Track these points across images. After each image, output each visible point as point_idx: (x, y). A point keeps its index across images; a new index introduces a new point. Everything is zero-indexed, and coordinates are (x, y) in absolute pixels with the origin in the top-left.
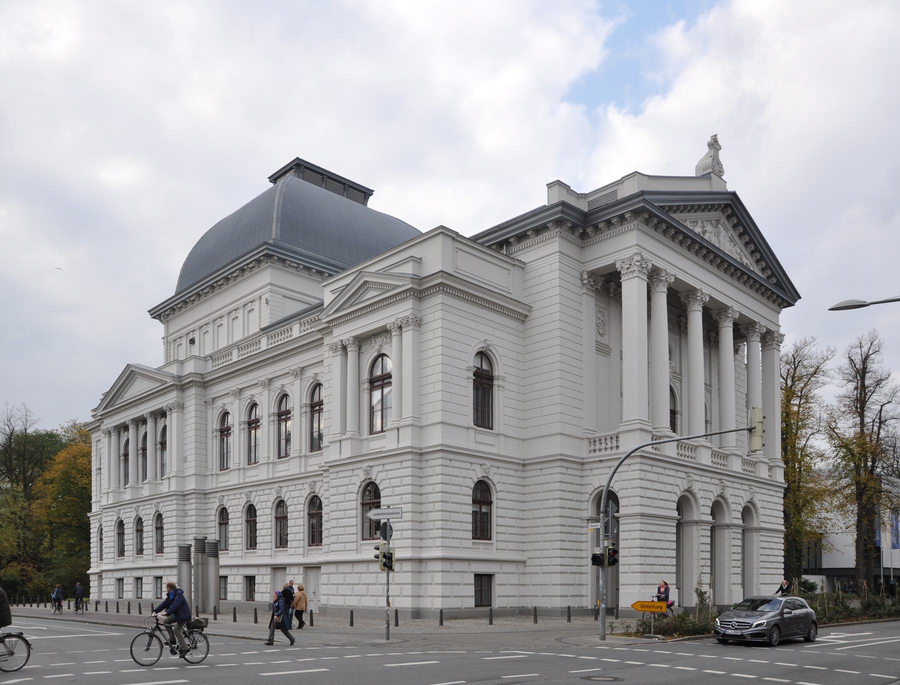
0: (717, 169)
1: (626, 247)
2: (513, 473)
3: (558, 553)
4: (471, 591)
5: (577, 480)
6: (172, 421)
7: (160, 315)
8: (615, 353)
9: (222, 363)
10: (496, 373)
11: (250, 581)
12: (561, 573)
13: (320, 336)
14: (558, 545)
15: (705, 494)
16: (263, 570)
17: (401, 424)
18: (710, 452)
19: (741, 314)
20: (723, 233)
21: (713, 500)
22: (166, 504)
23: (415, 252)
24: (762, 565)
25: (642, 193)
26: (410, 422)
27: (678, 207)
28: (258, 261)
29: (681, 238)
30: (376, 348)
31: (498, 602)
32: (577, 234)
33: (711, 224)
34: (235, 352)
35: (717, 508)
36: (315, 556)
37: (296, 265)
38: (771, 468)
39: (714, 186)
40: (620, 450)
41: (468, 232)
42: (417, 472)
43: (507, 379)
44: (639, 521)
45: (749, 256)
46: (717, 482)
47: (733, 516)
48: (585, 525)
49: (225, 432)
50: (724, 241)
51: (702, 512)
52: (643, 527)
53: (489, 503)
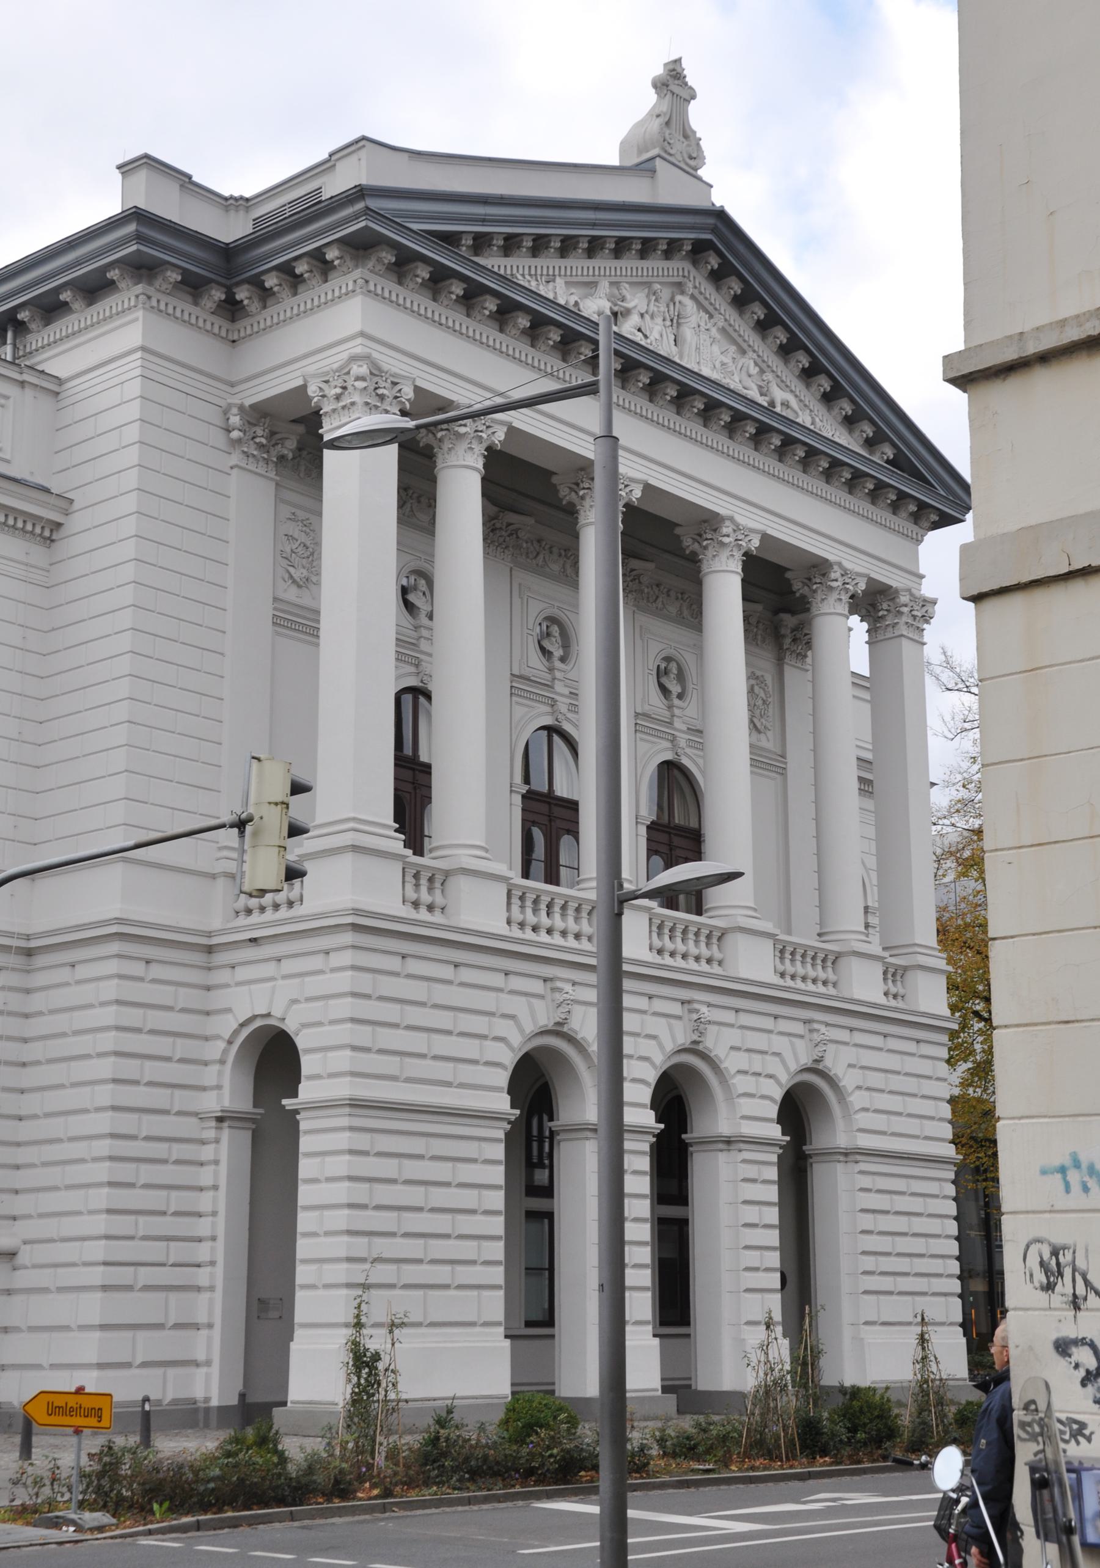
0: (679, 147)
1: (343, 337)
3: (100, 1224)
5: (186, 997)
12: (105, 1288)
14: (101, 1198)
24: (869, 1263)
32: (253, 306)
38: (894, 974)
39: (669, 189)
44: (345, 1122)
46: (676, 1009)
48: (211, 1134)
50: (709, 345)
52: (362, 1141)
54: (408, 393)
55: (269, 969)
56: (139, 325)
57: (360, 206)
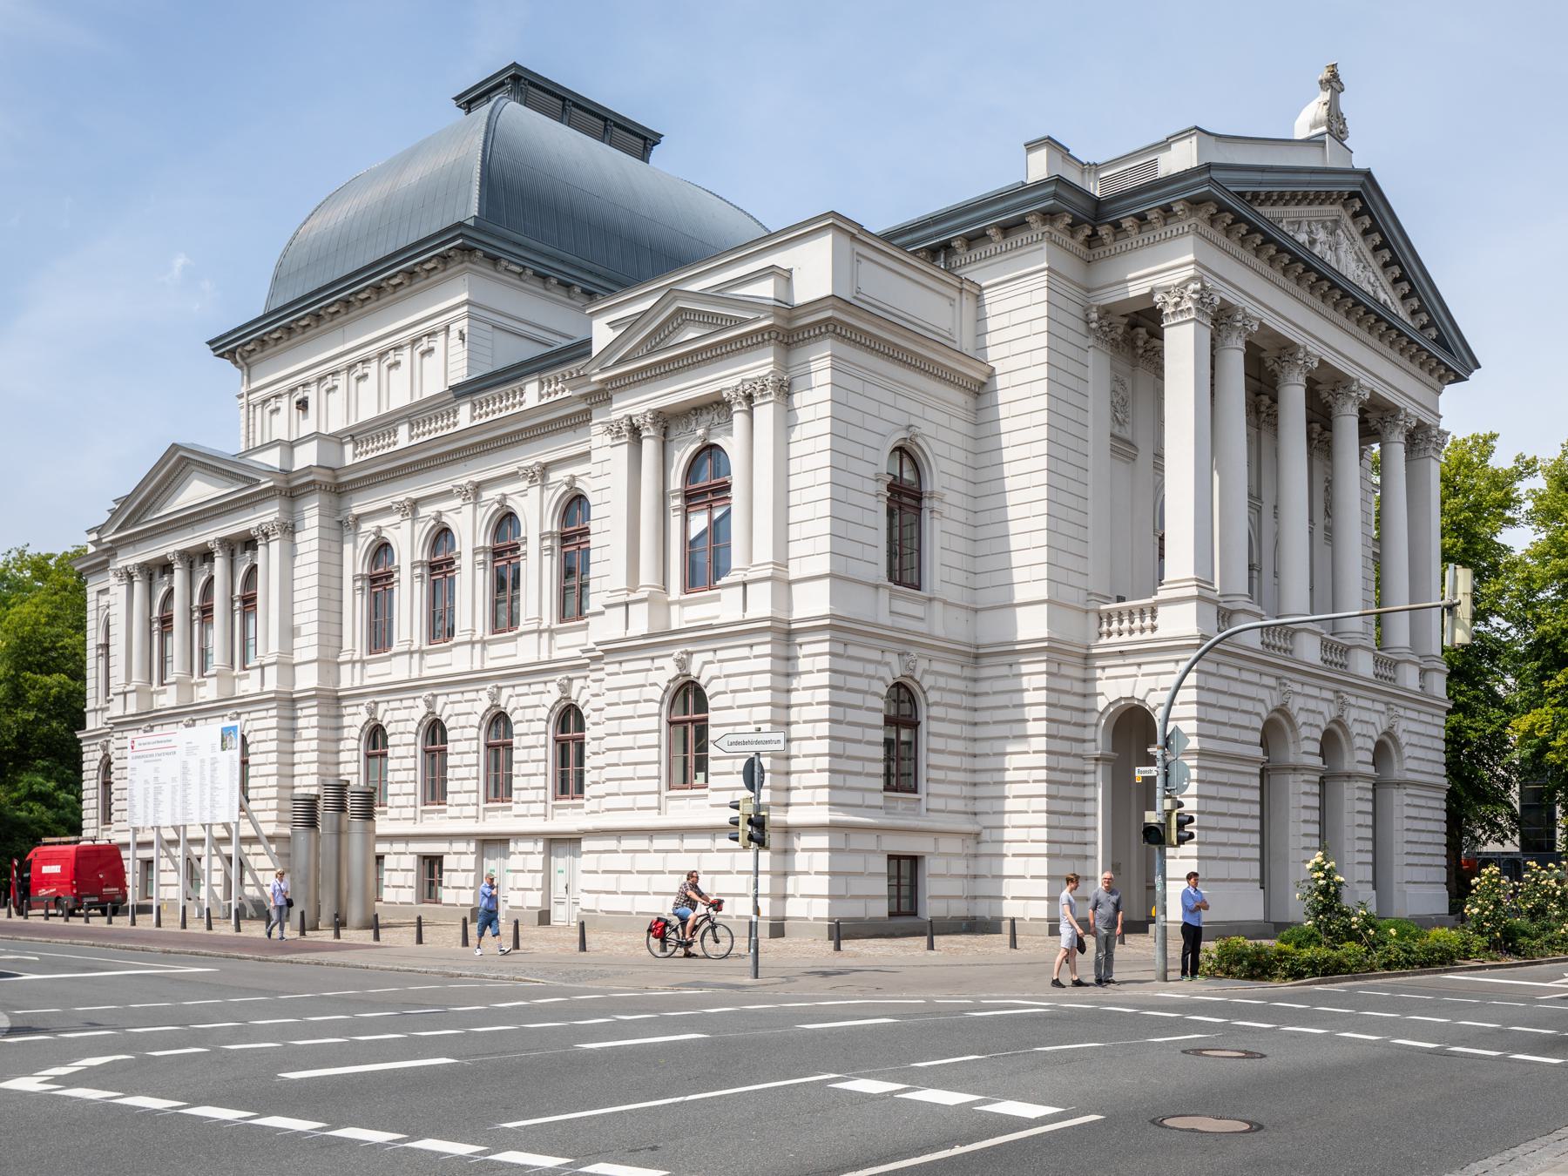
2: (956, 670)
4: (881, 886)
6: (269, 557)
7: (233, 352)
8: (1145, 458)
9: (375, 450)
10: (927, 487)
11: (432, 865)
13: (583, 406)
15: (1312, 711)
16: (460, 846)
17: (751, 576)
18: (1317, 641)
19: (1373, 393)
20: (1345, 244)
21: (1324, 727)
22: (253, 715)
23: (780, 259)
25: (1209, 167)
26: (768, 573)
27: (1269, 195)
28: (444, 259)
29: (1272, 251)
30: (700, 432)
31: (931, 909)
33: (1324, 227)
34: (403, 430)
35: (1331, 742)
36: (568, 819)
37: (518, 269)
38: (1423, 673)
39: (1331, 158)
40: (1157, 635)
41: (878, 223)
42: (782, 666)
43: (946, 499)
45: (1388, 288)
47: (1357, 758)
49: (379, 582)
50: (1351, 260)
51: (1304, 749)
53: (914, 725)
54: (1217, 301)
55: (1133, 670)
56: (1044, 253)
57: (1206, 176)
